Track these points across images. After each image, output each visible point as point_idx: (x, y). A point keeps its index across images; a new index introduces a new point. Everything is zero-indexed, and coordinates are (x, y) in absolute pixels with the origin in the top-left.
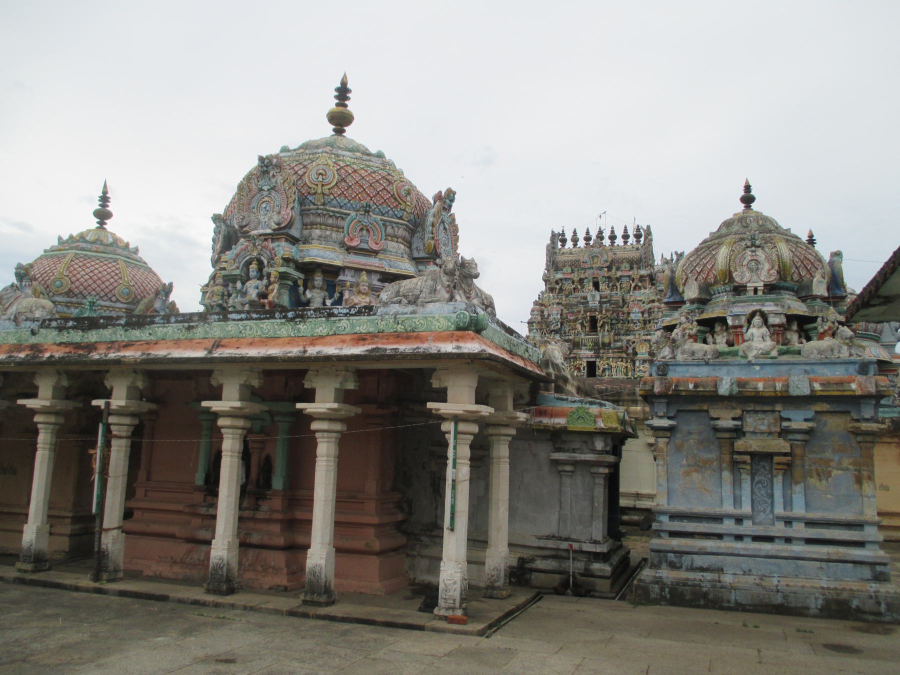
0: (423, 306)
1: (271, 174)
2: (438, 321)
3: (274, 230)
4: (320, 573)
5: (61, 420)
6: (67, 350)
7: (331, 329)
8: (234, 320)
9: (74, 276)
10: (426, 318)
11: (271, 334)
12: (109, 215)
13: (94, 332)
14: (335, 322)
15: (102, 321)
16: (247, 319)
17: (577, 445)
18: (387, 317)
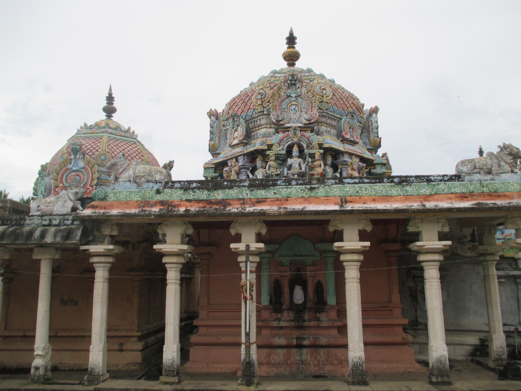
0: (497, 175)
1: (297, 86)
2: (512, 185)
3: (304, 124)
4: (445, 361)
5: (361, 258)
6: (201, 205)
7: (433, 190)
8: (349, 183)
9: (113, 153)
10: (503, 183)
11: (384, 193)
12: (114, 110)
13: (220, 192)
14: (434, 185)
15: (225, 183)
16: (359, 183)
17: (505, 266)
18: (474, 182)
